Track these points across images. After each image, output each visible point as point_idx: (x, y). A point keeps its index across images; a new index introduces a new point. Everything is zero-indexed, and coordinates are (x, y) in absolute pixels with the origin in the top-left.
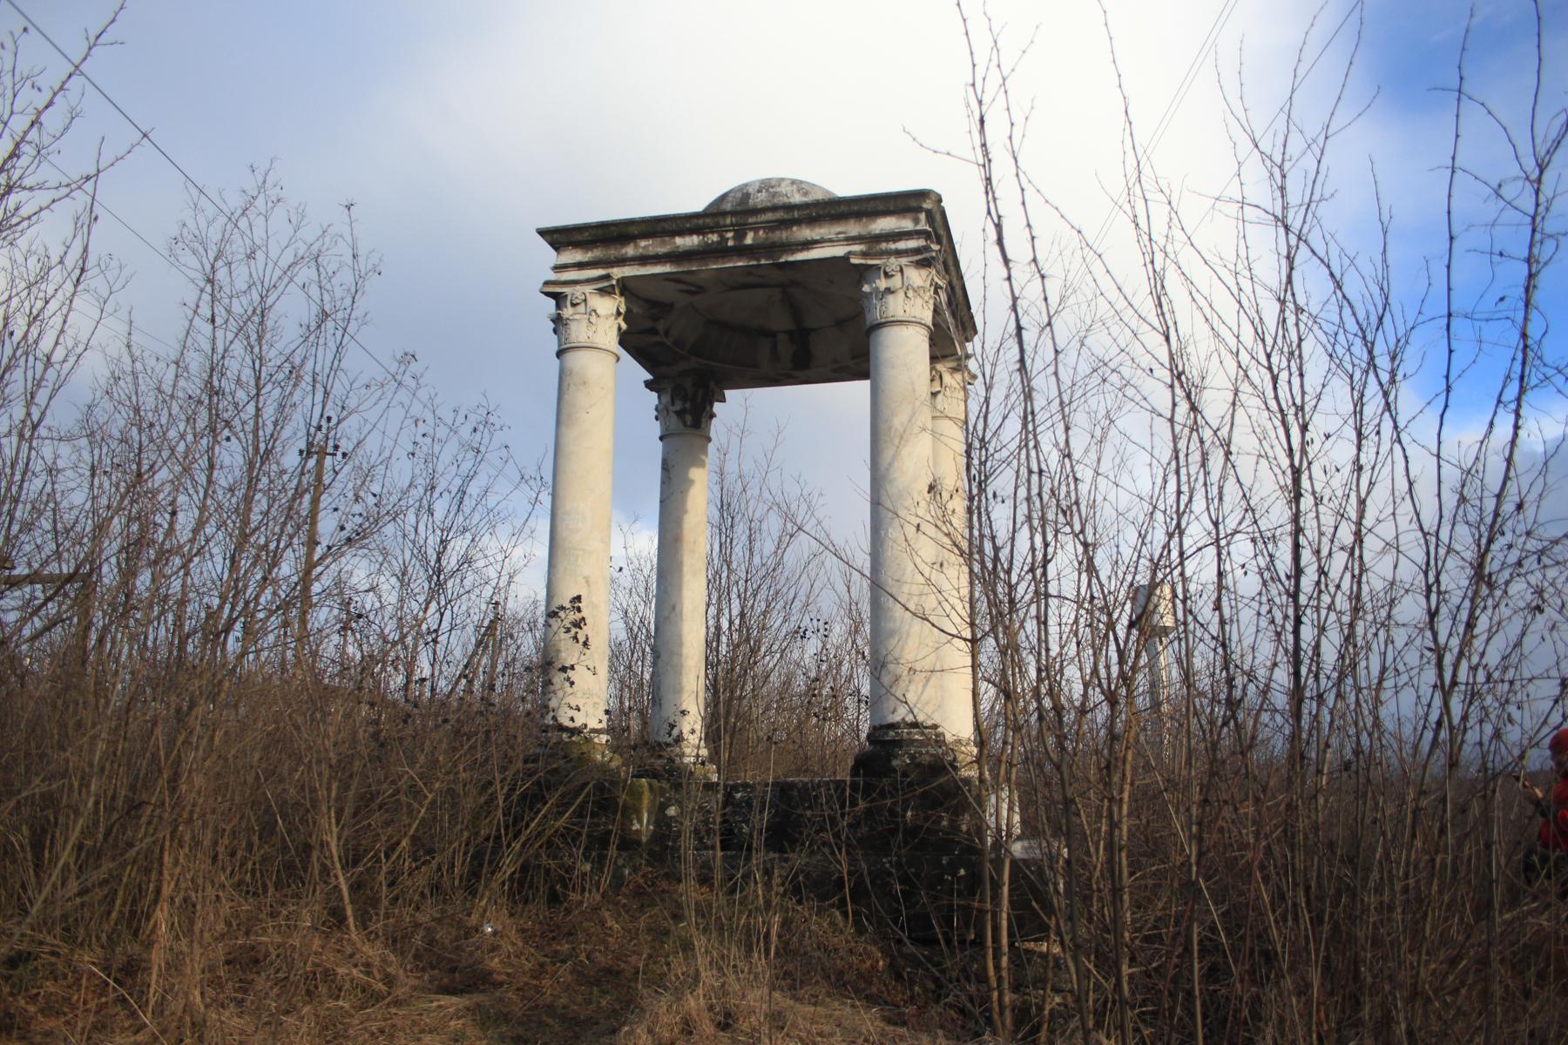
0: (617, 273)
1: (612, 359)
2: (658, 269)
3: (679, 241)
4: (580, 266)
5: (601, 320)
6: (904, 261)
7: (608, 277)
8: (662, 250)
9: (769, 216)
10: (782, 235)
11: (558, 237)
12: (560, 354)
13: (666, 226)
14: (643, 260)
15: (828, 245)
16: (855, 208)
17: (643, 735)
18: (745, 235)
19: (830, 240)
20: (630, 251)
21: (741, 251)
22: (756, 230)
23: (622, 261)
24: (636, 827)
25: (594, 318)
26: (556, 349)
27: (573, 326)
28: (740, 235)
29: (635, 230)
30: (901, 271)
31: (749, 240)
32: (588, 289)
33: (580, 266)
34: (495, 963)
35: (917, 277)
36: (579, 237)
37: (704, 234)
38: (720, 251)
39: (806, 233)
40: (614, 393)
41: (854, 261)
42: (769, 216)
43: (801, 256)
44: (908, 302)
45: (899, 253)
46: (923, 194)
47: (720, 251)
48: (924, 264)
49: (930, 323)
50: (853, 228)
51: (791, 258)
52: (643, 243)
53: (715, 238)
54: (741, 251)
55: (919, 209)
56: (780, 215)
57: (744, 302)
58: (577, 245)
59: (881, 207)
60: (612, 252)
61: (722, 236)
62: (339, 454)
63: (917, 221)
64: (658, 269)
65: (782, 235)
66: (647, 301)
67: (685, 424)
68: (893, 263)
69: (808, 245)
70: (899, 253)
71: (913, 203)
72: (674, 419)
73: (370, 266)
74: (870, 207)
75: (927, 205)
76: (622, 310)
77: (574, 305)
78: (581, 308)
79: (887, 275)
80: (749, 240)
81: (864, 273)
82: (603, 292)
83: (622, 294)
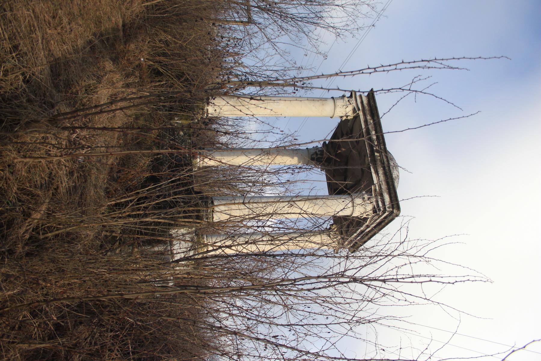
0: (361, 113)
1: (331, 115)
2: (363, 126)
3: (374, 132)
4: (362, 102)
5: (345, 110)
6: (374, 203)
7: (359, 110)
8: (370, 127)
9: (385, 160)
10: (379, 163)
11: (371, 95)
12: (333, 98)
13: (378, 128)
14: (366, 121)
15: (377, 178)
16: (391, 187)
17: (206, 135)
18: (378, 153)
19: (379, 179)
20: (369, 117)
21: (372, 152)
22: (380, 156)
23: (365, 115)
24: (176, 119)
25: (345, 107)
26: (334, 97)
27: (342, 101)
28: (378, 151)
29: (376, 118)
30: (371, 203)
31: (376, 154)
32: (354, 105)
33: (362, 102)
34: (132, 46)
35: (370, 207)
36: (371, 101)
37: (377, 140)
38: (371, 147)
39: (381, 172)
40: (320, 134)
41: (373, 187)
42: (385, 160)
43: (372, 170)
44: (358, 207)
45: (377, 202)
46: (398, 208)
47: (371, 147)
48: (375, 211)
49: (353, 215)
50: (384, 187)
51: (371, 167)
52: (371, 121)
53: (376, 143)
54: (372, 152)
55: (393, 208)
56: (386, 163)
57: (354, 158)
58: (369, 101)
59: (392, 195)
60: (367, 112)
61: (376, 146)
62: (295, 91)
63: (389, 208)
64: (363, 126)
65: (379, 163)
66: (352, 127)
67: (312, 155)
68: (374, 200)
69: (377, 173)
70: (377, 202)
71: (395, 206)
72: (313, 151)
73: (355, 34)
74: (392, 192)
75: (395, 211)
76: (349, 118)
77: (349, 101)
78: (348, 103)
79: (369, 199)
80: (376, 154)
81: (369, 192)
82: (354, 110)
83: (354, 117)
